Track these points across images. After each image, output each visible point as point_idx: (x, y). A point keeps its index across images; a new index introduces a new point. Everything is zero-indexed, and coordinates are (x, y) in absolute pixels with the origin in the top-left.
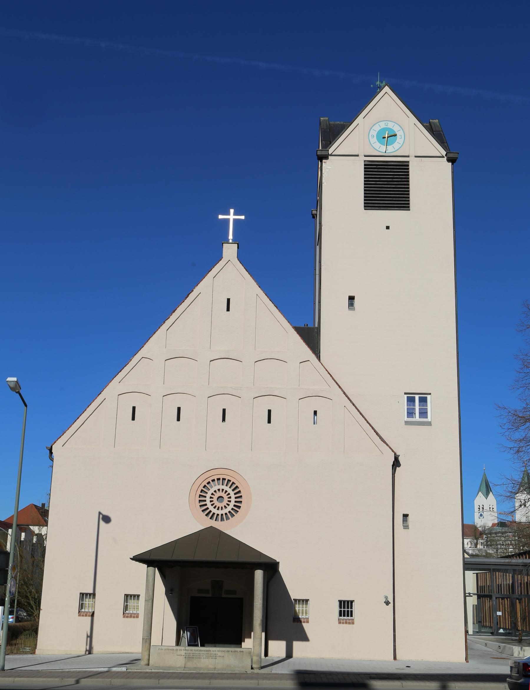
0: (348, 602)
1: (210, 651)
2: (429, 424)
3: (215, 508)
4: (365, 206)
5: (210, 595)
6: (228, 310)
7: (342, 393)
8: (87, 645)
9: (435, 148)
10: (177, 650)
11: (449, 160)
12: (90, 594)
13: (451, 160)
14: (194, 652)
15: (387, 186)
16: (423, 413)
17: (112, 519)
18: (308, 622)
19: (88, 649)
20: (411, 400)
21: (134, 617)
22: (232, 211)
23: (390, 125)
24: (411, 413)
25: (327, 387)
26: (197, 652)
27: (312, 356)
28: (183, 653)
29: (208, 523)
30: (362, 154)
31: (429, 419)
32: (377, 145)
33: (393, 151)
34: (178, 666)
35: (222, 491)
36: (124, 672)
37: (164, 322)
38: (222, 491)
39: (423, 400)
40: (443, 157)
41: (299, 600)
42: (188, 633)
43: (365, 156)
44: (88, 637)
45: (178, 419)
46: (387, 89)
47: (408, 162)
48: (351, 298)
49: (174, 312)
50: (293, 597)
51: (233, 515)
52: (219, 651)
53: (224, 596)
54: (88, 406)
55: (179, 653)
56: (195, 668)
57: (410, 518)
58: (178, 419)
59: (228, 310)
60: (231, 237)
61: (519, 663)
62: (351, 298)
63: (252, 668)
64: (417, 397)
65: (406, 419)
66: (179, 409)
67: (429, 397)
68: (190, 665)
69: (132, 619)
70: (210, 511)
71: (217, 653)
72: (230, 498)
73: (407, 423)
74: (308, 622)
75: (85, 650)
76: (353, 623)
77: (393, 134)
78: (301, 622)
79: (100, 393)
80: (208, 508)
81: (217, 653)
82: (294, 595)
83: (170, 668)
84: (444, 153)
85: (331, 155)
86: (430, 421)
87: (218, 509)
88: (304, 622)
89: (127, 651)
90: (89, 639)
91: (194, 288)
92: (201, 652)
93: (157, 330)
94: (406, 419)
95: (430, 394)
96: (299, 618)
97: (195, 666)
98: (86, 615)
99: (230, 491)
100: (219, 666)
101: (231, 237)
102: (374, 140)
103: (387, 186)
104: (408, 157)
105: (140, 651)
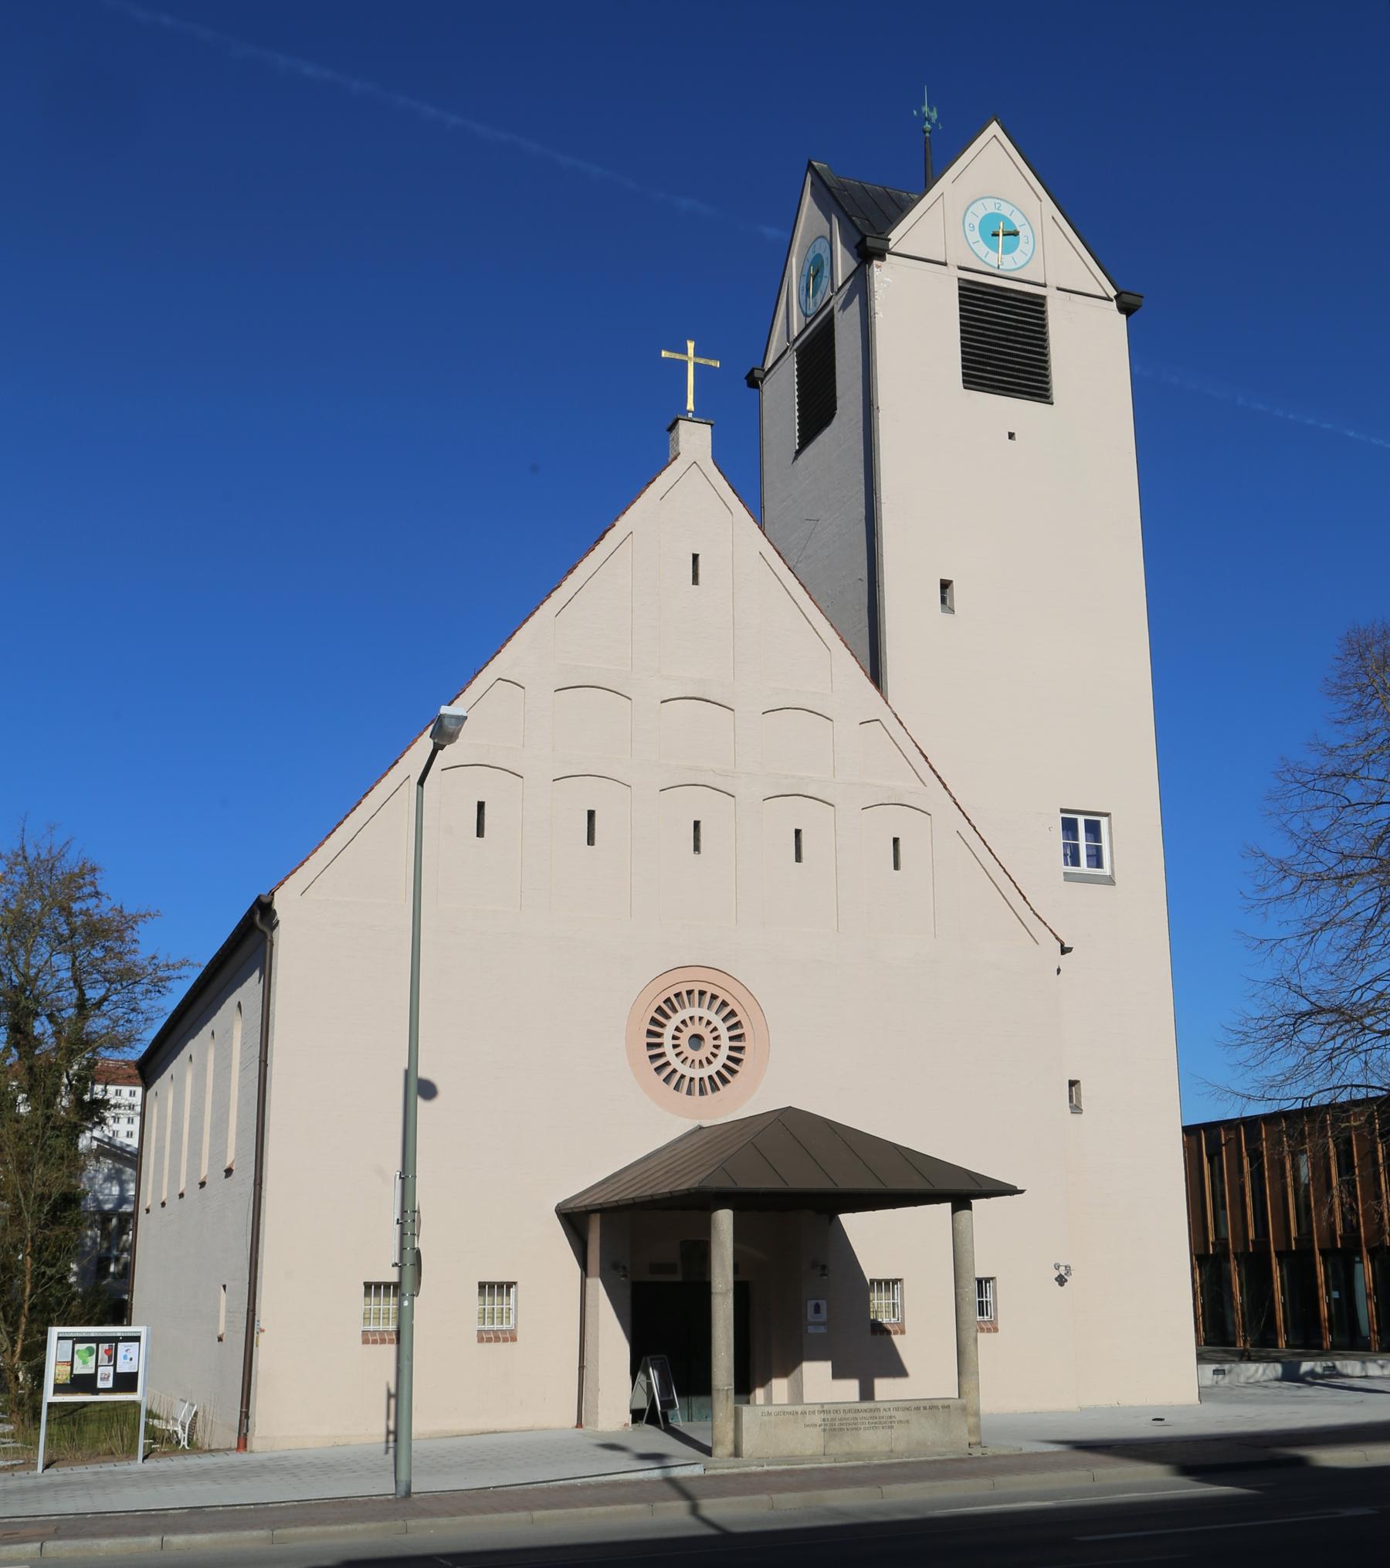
2: (1110, 881)
3: (715, 1055)
5: (678, 1278)
7: (950, 800)
8: (388, 1417)
9: (1096, 281)
11: (1122, 309)
12: (387, 1285)
13: (1126, 309)
14: (842, 1415)
15: (1004, 343)
16: (1096, 859)
17: (440, 1087)
18: (903, 1332)
19: (392, 1427)
20: (1069, 826)
21: (505, 1340)
22: (691, 345)
23: (1005, 210)
24: (1073, 858)
26: (849, 1415)
31: (1106, 870)
32: (982, 248)
33: (1010, 267)
34: (809, 1452)
35: (690, 1024)
36: (699, 1478)
37: (549, 596)
38: (690, 1024)
39: (1093, 829)
40: (1109, 299)
41: (879, 1282)
42: (654, 1374)
43: (960, 268)
44: (390, 1396)
46: (994, 128)
47: (1044, 298)
48: (945, 585)
49: (570, 572)
50: (868, 1276)
51: (725, 1081)
54: (366, 794)
56: (849, 1456)
60: (690, 406)
64: (1081, 820)
67: (1104, 821)
68: (835, 1447)
69: (501, 1345)
71: (893, 1413)
74: (903, 1332)
75: (384, 1431)
76: (996, 1330)
77: (1011, 230)
78: (888, 1332)
79: (396, 762)
80: (667, 1064)
81: (893, 1413)
82: (870, 1273)
83: (789, 1459)
84: (1113, 293)
86: (1108, 873)
87: (709, 1062)
88: (896, 1333)
89: (491, 1427)
90: (393, 1402)
91: (617, 520)
92: (858, 1415)
93: (532, 614)
95: (1107, 815)
96: (881, 1324)
97: (847, 1449)
98: (383, 1341)
99: (717, 1021)
100: (900, 1446)
101: (690, 406)
102: (974, 236)
103: (1004, 343)
104: (1044, 286)
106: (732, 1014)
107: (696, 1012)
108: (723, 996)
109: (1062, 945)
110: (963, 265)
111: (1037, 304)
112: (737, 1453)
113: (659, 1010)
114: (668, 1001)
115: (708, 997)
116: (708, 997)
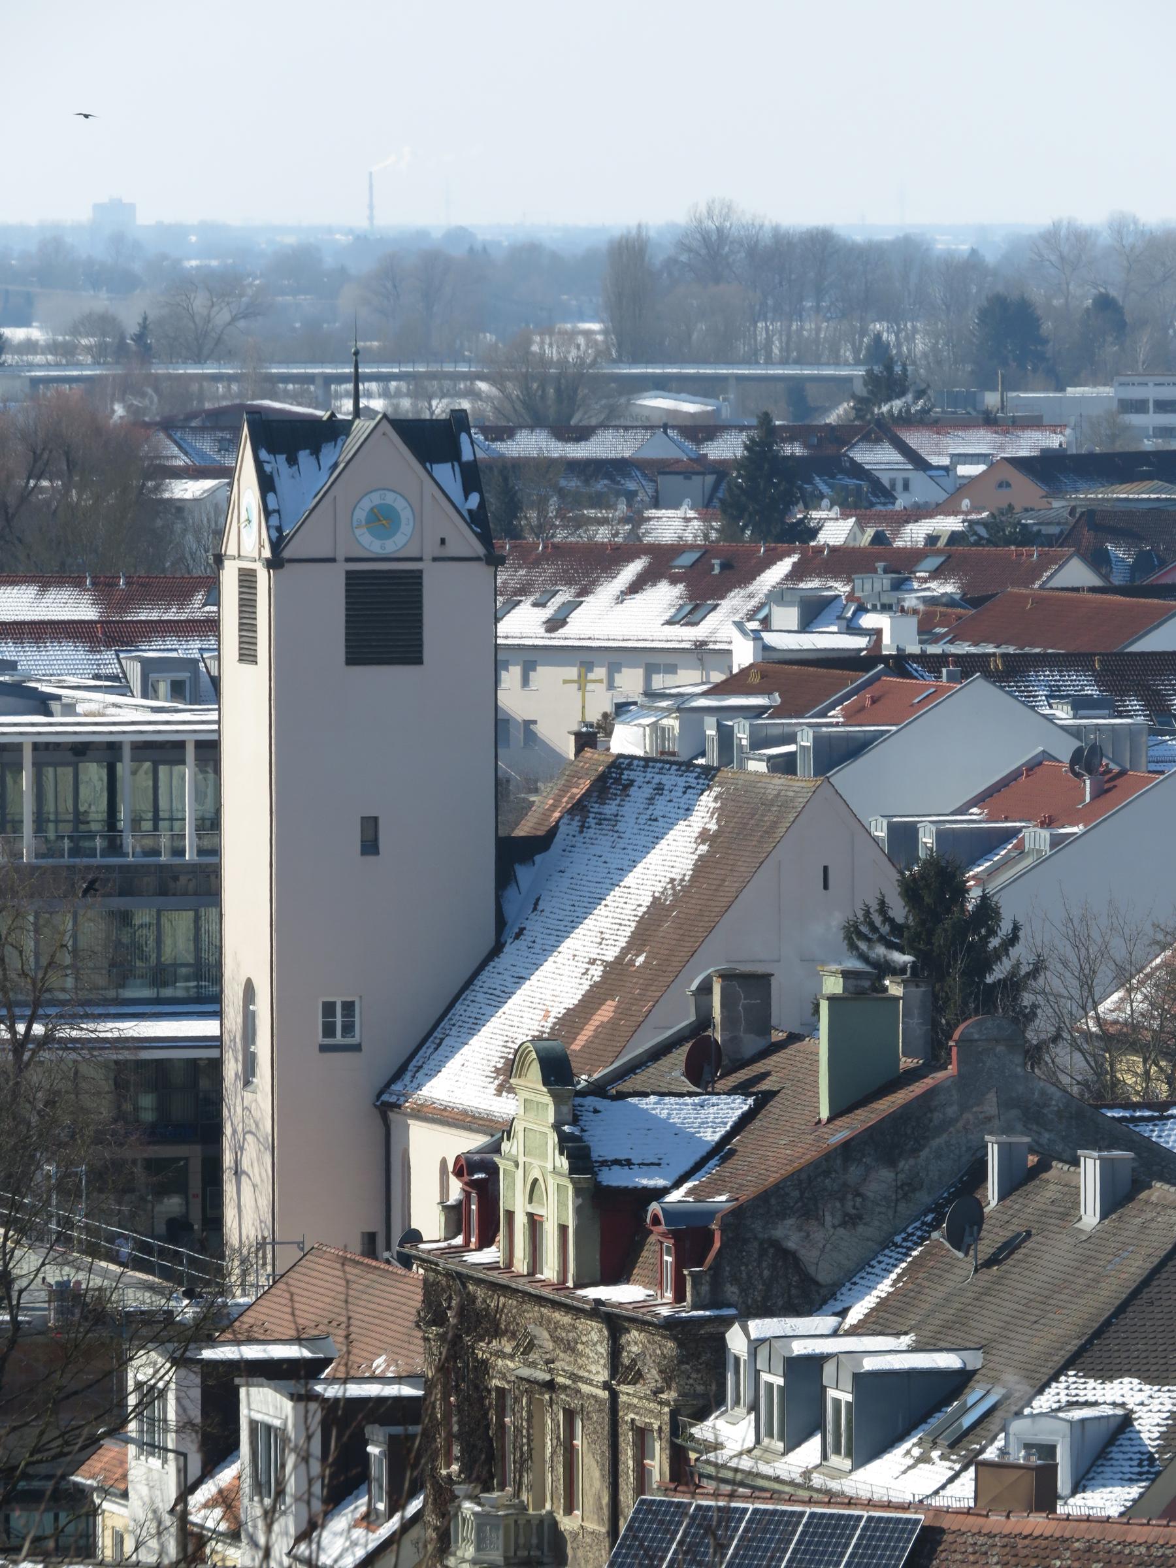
2: (357, 1048)
30: (341, 556)
43: (348, 560)
48: (370, 846)
73: (323, 1049)
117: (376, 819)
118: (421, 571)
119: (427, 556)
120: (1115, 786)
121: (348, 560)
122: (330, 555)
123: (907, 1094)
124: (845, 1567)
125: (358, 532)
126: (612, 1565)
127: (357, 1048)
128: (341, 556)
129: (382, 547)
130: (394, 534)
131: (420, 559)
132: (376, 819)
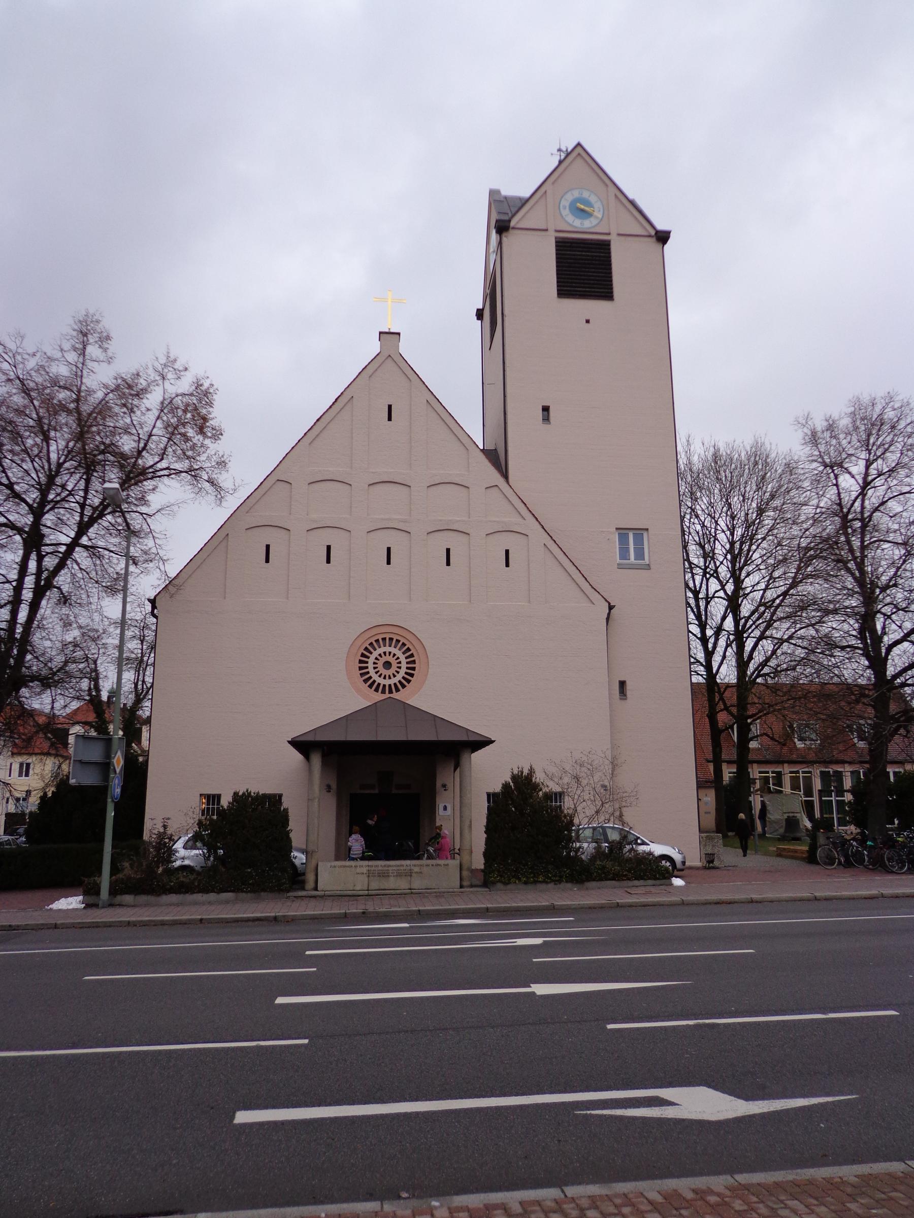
0: (214, 796)
1: (402, 866)
2: (648, 567)
4: (559, 294)
5: (376, 791)
6: (390, 419)
7: (540, 527)
10: (356, 867)
14: (380, 868)
16: (640, 554)
25: (521, 520)
27: (500, 481)
28: (365, 870)
29: (379, 697)
30: (551, 228)
32: (570, 218)
35: (387, 655)
38: (387, 655)
43: (557, 231)
45: (328, 561)
47: (609, 241)
48: (546, 409)
51: (370, 686)
52: (415, 866)
53: (394, 791)
55: (359, 870)
57: (629, 686)
58: (328, 561)
59: (390, 419)
61: (304, 874)
62: (546, 409)
63: (461, 887)
65: (618, 561)
66: (329, 548)
70: (374, 681)
72: (374, 663)
73: (620, 566)
85: (513, 228)
94: (618, 561)
95: (647, 530)
102: (566, 212)
105: (482, 867)
106: (409, 650)
107: (387, 649)
108: (402, 640)
109: (609, 604)
110: (558, 229)
111: (604, 247)
112: (316, 889)
113: (366, 649)
114: (371, 644)
115: (375, 643)
116: (375, 643)
117: (380, 333)
118: (609, 241)
119: (614, 233)
120: (607, 185)
121: (557, 231)
122: (544, 227)
123: (912, 698)
124: (4, 1059)
125: (600, 216)
126: (911, 871)
127: (648, 567)
128: (551, 228)
129: (565, 208)
130: (573, 214)
131: (609, 234)
132: (380, 333)
